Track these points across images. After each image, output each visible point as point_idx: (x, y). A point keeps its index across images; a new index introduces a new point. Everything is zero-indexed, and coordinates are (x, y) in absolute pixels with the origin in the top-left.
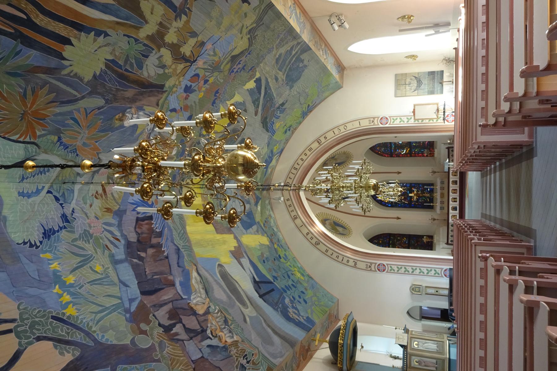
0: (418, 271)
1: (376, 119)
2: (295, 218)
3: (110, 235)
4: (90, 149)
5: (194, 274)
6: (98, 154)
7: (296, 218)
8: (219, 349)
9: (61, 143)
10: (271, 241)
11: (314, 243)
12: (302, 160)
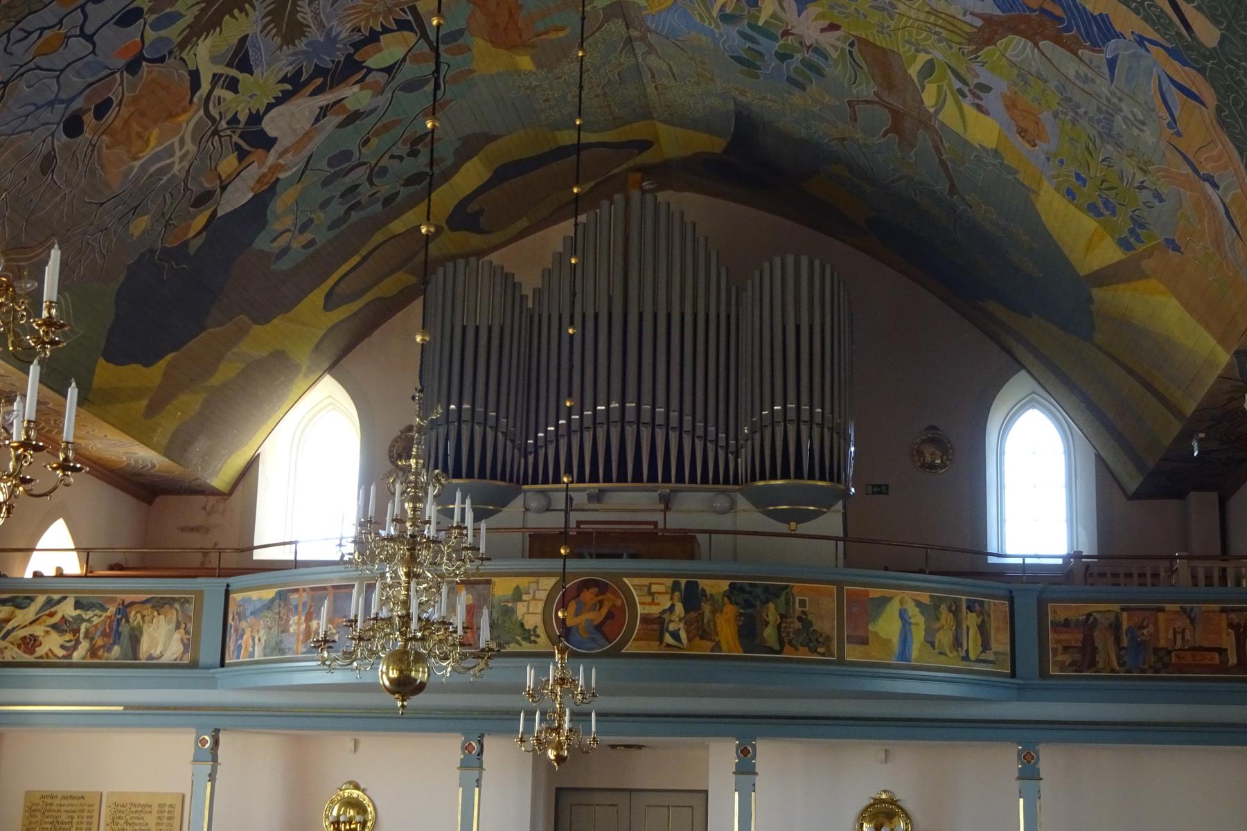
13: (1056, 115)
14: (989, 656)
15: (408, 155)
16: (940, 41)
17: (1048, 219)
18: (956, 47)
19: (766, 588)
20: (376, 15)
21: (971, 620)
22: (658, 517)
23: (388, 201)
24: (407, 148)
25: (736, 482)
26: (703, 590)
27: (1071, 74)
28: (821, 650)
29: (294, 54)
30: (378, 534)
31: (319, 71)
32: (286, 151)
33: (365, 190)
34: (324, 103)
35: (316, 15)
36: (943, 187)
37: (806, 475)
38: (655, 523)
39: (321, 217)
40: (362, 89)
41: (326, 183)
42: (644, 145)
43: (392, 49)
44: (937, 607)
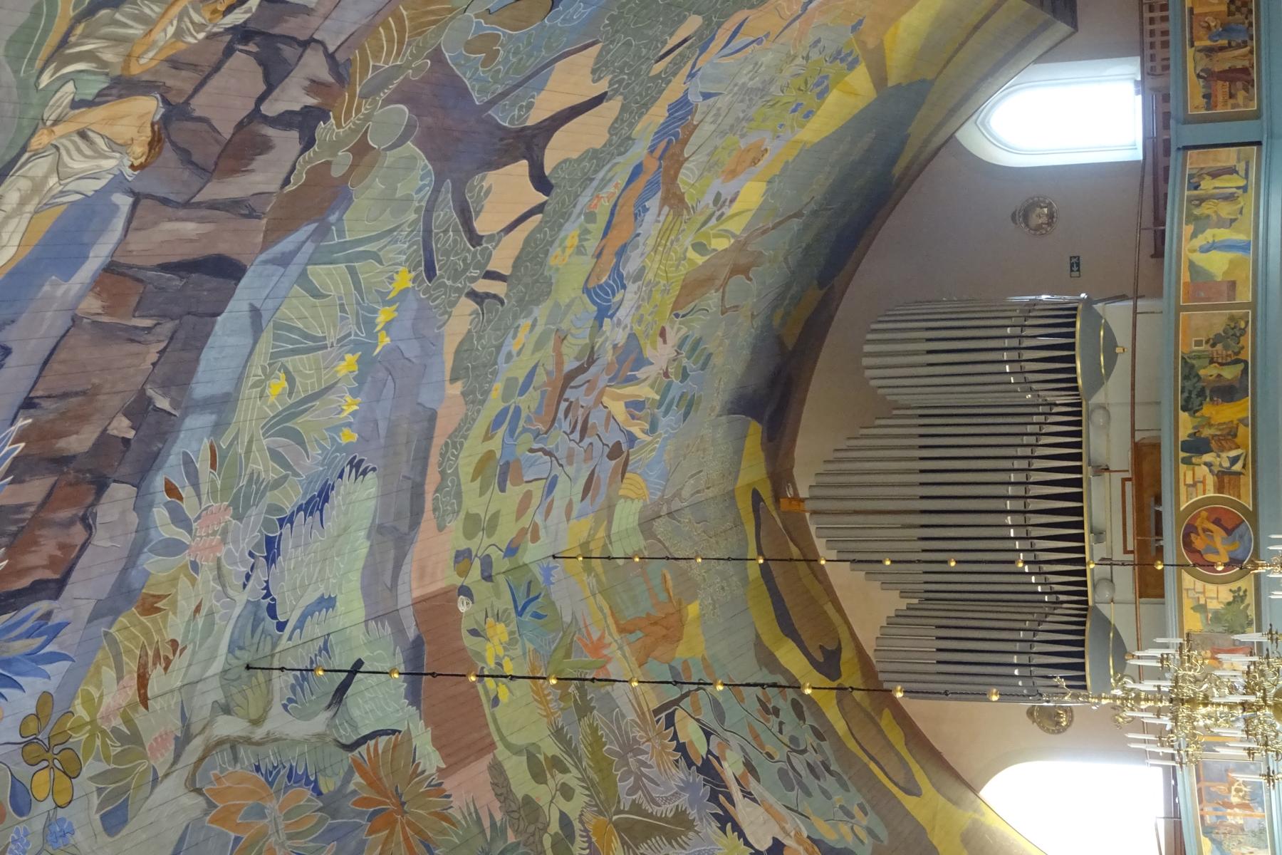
4: (239, 807)
6: (211, 805)
9: (308, 783)
13: (742, 136)
14: (1241, 167)
15: (777, 716)
16: (677, 240)
17: (828, 130)
18: (684, 226)
19: (1185, 378)
20: (664, 747)
21: (1208, 185)
22: (1117, 478)
23: (819, 736)
24: (772, 717)
25: (1080, 405)
26: (1190, 436)
27: (713, 127)
28: (1243, 325)
29: (701, 819)
30: (1172, 731)
31: (713, 798)
32: (783, 829)
33: (811, 756)
34: (740, 794)
35: (667, 800)
36: (795, 224)
37: (1071, 340)
38: (1124, 480)
39: (839, 798)
40: (725, 759)
41: (808, 794)
42: (756, 498)
43: (690, 732)
44: (1197, 218)
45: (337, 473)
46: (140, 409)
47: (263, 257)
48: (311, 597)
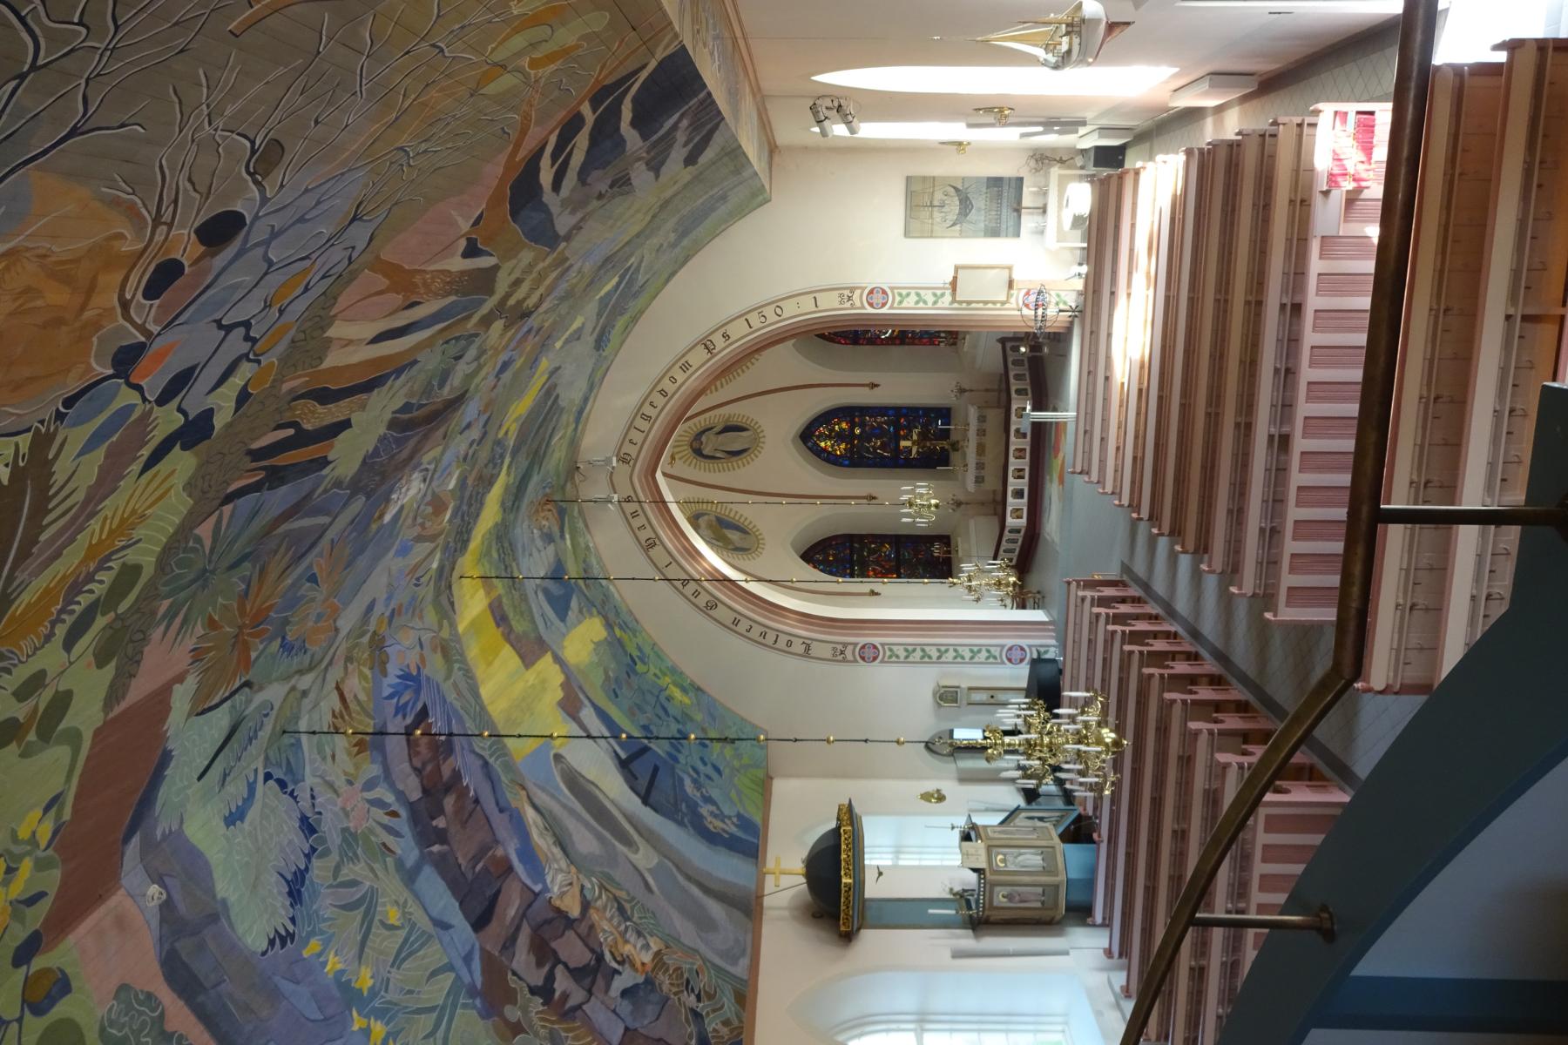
0: (951, 654)
1: (857, 292)
2: (650, 545)
3: (381, 812)
5: (530, 814)
7: (652, 545)
8: (641, 993)
10: (609, 626)
11: (702, 604)
12: (663, 393)
45: (298, 921)
46: (442, 836)
47: (477, 946)
48: (253, 814)
